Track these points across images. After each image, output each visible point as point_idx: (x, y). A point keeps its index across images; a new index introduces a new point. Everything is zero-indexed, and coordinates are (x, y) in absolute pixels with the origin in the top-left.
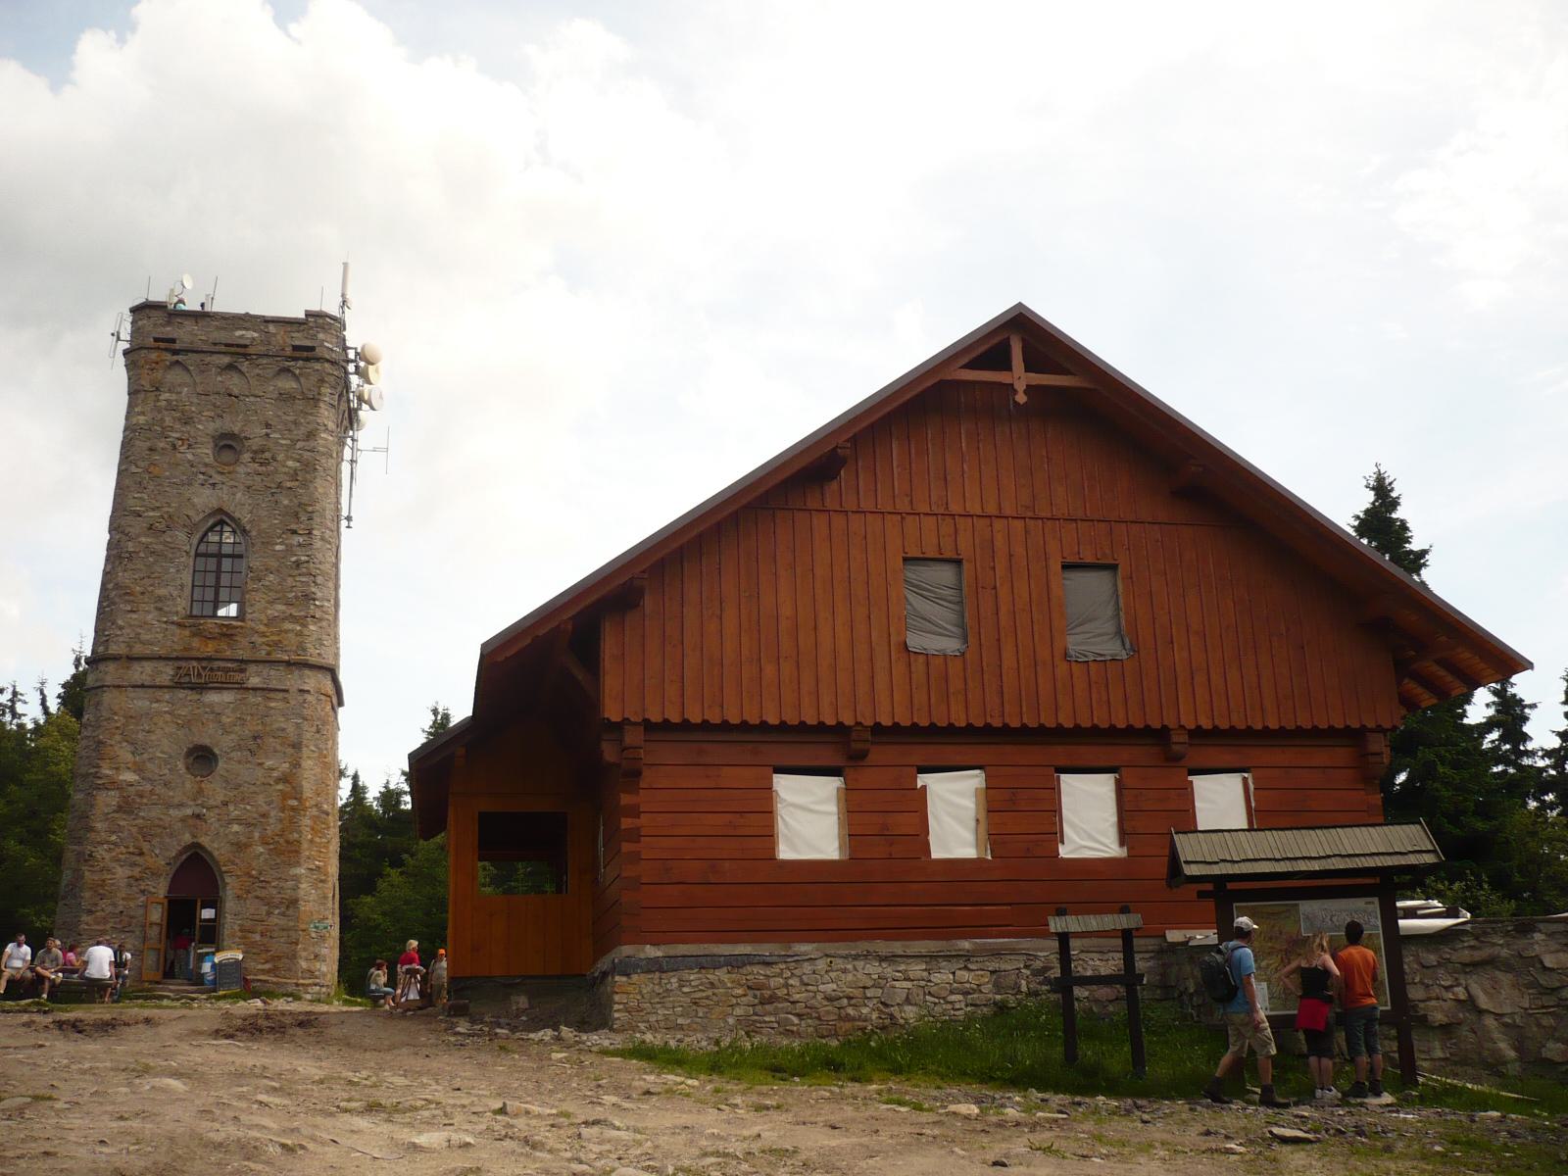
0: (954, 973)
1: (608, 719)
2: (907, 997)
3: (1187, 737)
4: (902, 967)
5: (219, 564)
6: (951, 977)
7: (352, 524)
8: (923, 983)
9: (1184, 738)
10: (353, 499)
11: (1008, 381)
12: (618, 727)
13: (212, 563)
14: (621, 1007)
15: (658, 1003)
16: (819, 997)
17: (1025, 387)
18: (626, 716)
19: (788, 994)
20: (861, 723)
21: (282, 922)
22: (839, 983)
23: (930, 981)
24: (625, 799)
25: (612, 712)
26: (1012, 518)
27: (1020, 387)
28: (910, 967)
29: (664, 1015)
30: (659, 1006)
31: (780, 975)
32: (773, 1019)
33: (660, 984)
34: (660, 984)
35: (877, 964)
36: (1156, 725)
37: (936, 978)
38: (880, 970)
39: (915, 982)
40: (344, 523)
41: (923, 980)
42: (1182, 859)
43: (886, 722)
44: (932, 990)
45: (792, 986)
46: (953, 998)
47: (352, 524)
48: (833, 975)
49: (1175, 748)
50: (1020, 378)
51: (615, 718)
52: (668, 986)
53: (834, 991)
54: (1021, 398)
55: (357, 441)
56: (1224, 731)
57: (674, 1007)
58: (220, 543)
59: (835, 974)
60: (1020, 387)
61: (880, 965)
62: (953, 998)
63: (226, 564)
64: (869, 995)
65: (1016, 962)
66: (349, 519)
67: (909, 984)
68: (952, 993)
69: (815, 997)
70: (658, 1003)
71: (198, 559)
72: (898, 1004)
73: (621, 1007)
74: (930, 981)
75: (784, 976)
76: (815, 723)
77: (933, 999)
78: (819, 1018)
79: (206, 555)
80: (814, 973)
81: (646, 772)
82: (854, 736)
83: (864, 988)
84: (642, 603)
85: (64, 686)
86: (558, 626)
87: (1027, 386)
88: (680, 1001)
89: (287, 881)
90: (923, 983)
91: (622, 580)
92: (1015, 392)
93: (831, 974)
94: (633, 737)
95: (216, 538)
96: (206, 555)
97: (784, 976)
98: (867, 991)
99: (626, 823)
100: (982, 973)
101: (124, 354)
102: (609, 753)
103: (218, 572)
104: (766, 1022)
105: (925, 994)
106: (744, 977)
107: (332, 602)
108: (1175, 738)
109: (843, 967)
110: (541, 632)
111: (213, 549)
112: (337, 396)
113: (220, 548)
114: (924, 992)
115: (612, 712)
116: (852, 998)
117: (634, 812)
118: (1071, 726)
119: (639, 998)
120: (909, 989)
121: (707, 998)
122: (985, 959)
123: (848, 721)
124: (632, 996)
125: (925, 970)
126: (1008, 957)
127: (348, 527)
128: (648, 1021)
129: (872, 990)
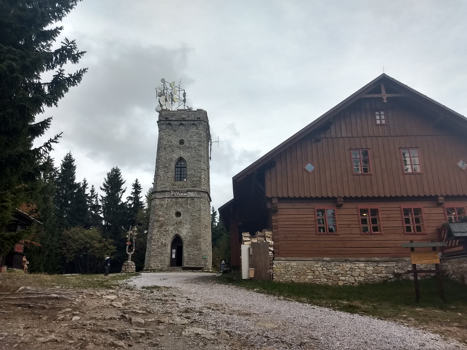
0: (373, 267)
1: (268, 197)
2: (360, 274)
3: (444, 198)
4: (357, 265)
5: (181, 170)
6: (373, 268)
7: (211, 159)
8: (364, 270)
9: (443, 198)
10: (211, 155)
11: (381, 96)
12: (270, 199)
13: (179, 169)
14: (275, 275)
15: (285, 274)
16: (333, 273)
17: (386, 98)
18: (272, 196)
19: (323, 272)
20: (340, 196)
21: (197, 252)
22: (338, 269)
23: (366, 269)
24: (274, 218)
25: (268, 195)
26: (384, 136)
27: (385, 98)
28: (360, 265)
29: (287, 277)
30: (286, 275)
31: (320, 267)
32: (319, 280)
33: (286, 268)
34: (286, 268)
35: (350, 264)
36: (433, 195)
37: (368, 268)
38: (350, 266)
39: (361, 270)
40: (210, 159)
41: (364, 269)
42: (453, 231)
43: (348, 196)
44: (367, 272)
45: (324, 270)
46: (374, 275)
47: (211, 159)
48: (336, 267)
49: (440, 201)
50: (384, 96)
51: (270, 196)
52: (288, 269)
53: (337, 272)
54: (385, 101)
55: (211, 140)
56: (456, 196)
57: (290, 275)
58: (181, 164)
59: (337, 267)
60: (385, 98)
61: (351, 264)
62: (374, 275)
63: (182, 169)
64: (347, 273)
65: (393, 264)
66: (210, 158)
67: (359, 270)
68: (373, 273)
69: (331, 274)
70: (285, 274)
71: (176, 168)
72: (357, 276)
73: (275, 275)
74: (366, 269)
75: (322, 267)
76: (326, 197)
77: (367, 275)
78: (333, 280)
79: (178, 167)
80: (331, 266)
81: (279, 210)
82: (338, 200)
83: (346, 271)
84: (275, 166)
85: (75, 167)
86: (253, 172)
87: (387, 97)
88: (292, 274)
89: (198, 242)
90: (364, 270)
91: (269, 159)
92: (383, 99)
93: (336, 267)
94: (275, 201)
95: (180, 163)
96: (178, 167)
97: (322, 267)
98: (347, 272)
99: (274, 224)
100: (382, 267)
101: (157, 122)
102: (269, 206)
103: (181, 171)
104: (317, 280)
105: (365, 273)
106: (310, 267)
107: (207, 177)
108: (440, 198)
109: (339, 265)
110: (249, 173)
111: (179, 166)
112: (206, 129)
113: (181, 165)
114: (365, 273)
115: (268, 195)
116: (343, 274)
117: (277, 221)
118: (406, 196)
119: (280, 272)
120: (360, 272)
121: (300, 273)
122: (383, 263)
123: (336, 195)
124: (278, 272)
125: (364, 266)
126: (390, 262)
127: (210, 160)
128: (283, 279)
129: (348, 272)
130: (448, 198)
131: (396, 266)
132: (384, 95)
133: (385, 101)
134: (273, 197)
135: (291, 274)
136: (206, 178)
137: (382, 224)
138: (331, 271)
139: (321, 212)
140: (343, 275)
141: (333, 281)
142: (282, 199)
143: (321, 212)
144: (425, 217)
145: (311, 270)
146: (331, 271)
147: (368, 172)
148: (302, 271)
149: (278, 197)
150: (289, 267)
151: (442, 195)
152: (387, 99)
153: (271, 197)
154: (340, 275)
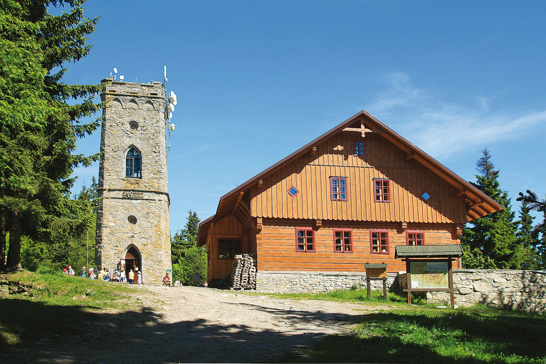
1: (253, 216)
25: (254, 215)
52: (270, 280)
54: (363, 136)
60: (363, 133)
98: (320, 283)
123: (316, 218)
130: (411, 225)
131: (361, 279)
132: (133, 220)
133: (363, 136)
134: (258, 217)
135: (272, 284)
136: (270, 168)
137: (354, 244)
138: (307, 282)
139: (405, 262)
140: (316, 285)
141: (308, 290)
142: (268, 221)
143: (405, 262)
144: (390, 240)
145: (290, 281)
146: (307, 282)
147: (380, 200)
148: (281, 282)
149: (263, 217)
150: (271, 279)
151: (405, 222)
152: (366, 133)
153: (256, 216)
154: (314, 285)
